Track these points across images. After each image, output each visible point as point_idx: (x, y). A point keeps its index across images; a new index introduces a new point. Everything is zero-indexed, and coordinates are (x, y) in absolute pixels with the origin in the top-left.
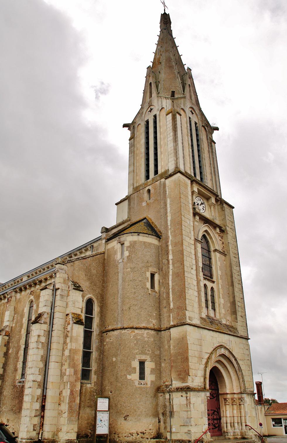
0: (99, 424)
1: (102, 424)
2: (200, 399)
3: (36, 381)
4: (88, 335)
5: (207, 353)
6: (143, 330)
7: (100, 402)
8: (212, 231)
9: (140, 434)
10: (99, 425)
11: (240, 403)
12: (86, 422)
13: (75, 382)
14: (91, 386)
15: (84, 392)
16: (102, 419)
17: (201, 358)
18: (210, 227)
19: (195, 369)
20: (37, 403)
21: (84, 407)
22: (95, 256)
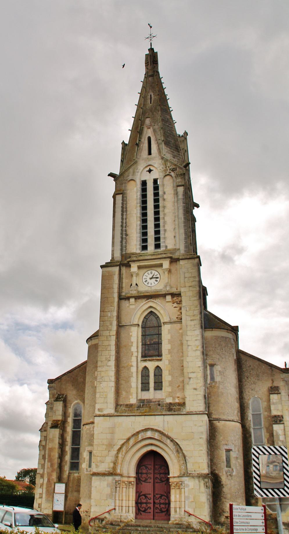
0: (56, 502)
1: (59, 503)
2: (105, 483)
3: (39, 474)
4: (62, 437)
5: (122, 439)
6: (91, 425)
7: (58, 487)
8: (158, 304)
9: (85, 512)
10: (56, 504)
11: (116, 485)
12: (74, 503)
13: (52, 473)
14: (78, 475)
15: (71, 480)
16: (58, 499)
17: (110, 446)
18: (153, 302)
19: (102, 456)
20: (40, 489)
21: (72, 491)
22: (82, 366)
